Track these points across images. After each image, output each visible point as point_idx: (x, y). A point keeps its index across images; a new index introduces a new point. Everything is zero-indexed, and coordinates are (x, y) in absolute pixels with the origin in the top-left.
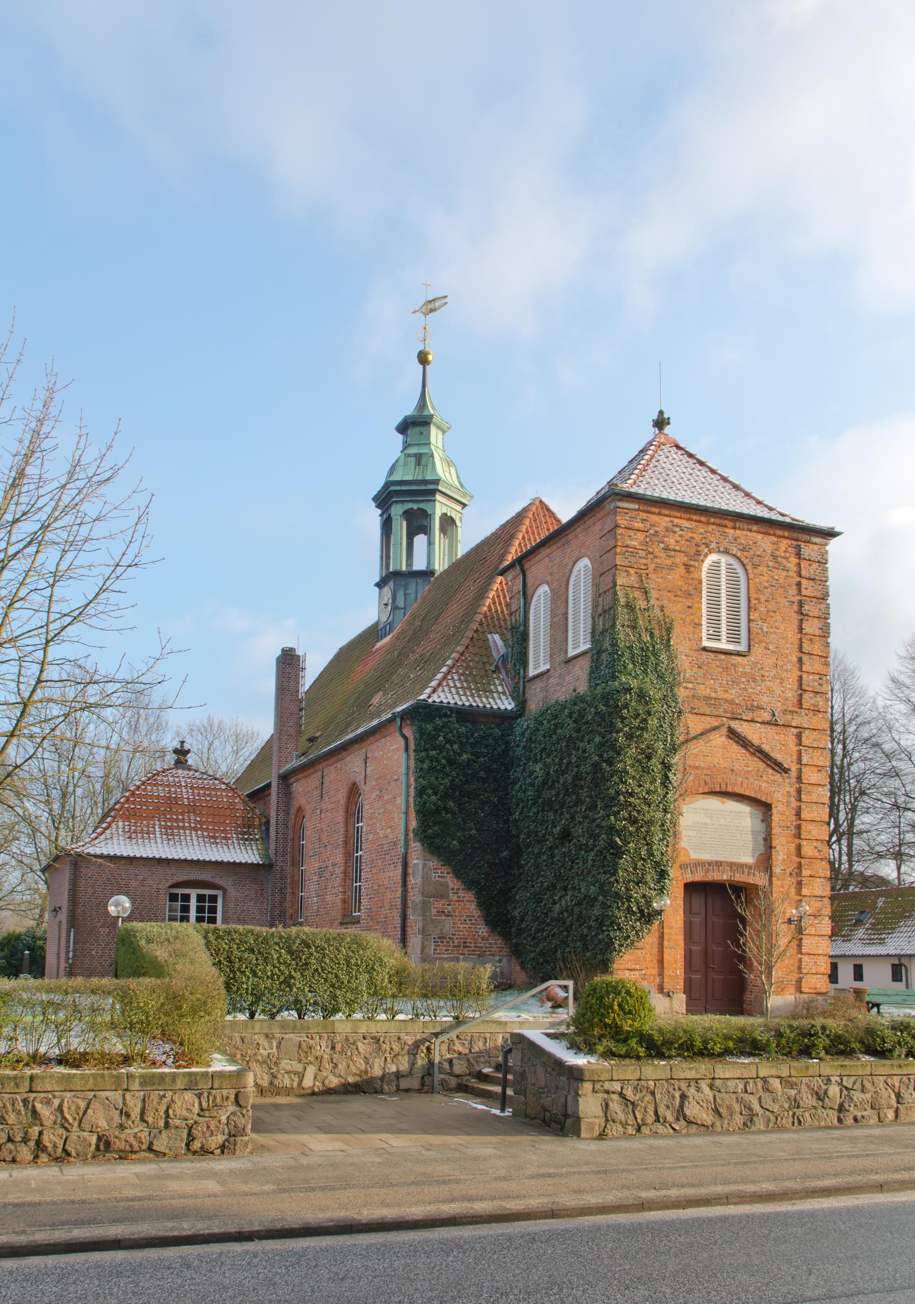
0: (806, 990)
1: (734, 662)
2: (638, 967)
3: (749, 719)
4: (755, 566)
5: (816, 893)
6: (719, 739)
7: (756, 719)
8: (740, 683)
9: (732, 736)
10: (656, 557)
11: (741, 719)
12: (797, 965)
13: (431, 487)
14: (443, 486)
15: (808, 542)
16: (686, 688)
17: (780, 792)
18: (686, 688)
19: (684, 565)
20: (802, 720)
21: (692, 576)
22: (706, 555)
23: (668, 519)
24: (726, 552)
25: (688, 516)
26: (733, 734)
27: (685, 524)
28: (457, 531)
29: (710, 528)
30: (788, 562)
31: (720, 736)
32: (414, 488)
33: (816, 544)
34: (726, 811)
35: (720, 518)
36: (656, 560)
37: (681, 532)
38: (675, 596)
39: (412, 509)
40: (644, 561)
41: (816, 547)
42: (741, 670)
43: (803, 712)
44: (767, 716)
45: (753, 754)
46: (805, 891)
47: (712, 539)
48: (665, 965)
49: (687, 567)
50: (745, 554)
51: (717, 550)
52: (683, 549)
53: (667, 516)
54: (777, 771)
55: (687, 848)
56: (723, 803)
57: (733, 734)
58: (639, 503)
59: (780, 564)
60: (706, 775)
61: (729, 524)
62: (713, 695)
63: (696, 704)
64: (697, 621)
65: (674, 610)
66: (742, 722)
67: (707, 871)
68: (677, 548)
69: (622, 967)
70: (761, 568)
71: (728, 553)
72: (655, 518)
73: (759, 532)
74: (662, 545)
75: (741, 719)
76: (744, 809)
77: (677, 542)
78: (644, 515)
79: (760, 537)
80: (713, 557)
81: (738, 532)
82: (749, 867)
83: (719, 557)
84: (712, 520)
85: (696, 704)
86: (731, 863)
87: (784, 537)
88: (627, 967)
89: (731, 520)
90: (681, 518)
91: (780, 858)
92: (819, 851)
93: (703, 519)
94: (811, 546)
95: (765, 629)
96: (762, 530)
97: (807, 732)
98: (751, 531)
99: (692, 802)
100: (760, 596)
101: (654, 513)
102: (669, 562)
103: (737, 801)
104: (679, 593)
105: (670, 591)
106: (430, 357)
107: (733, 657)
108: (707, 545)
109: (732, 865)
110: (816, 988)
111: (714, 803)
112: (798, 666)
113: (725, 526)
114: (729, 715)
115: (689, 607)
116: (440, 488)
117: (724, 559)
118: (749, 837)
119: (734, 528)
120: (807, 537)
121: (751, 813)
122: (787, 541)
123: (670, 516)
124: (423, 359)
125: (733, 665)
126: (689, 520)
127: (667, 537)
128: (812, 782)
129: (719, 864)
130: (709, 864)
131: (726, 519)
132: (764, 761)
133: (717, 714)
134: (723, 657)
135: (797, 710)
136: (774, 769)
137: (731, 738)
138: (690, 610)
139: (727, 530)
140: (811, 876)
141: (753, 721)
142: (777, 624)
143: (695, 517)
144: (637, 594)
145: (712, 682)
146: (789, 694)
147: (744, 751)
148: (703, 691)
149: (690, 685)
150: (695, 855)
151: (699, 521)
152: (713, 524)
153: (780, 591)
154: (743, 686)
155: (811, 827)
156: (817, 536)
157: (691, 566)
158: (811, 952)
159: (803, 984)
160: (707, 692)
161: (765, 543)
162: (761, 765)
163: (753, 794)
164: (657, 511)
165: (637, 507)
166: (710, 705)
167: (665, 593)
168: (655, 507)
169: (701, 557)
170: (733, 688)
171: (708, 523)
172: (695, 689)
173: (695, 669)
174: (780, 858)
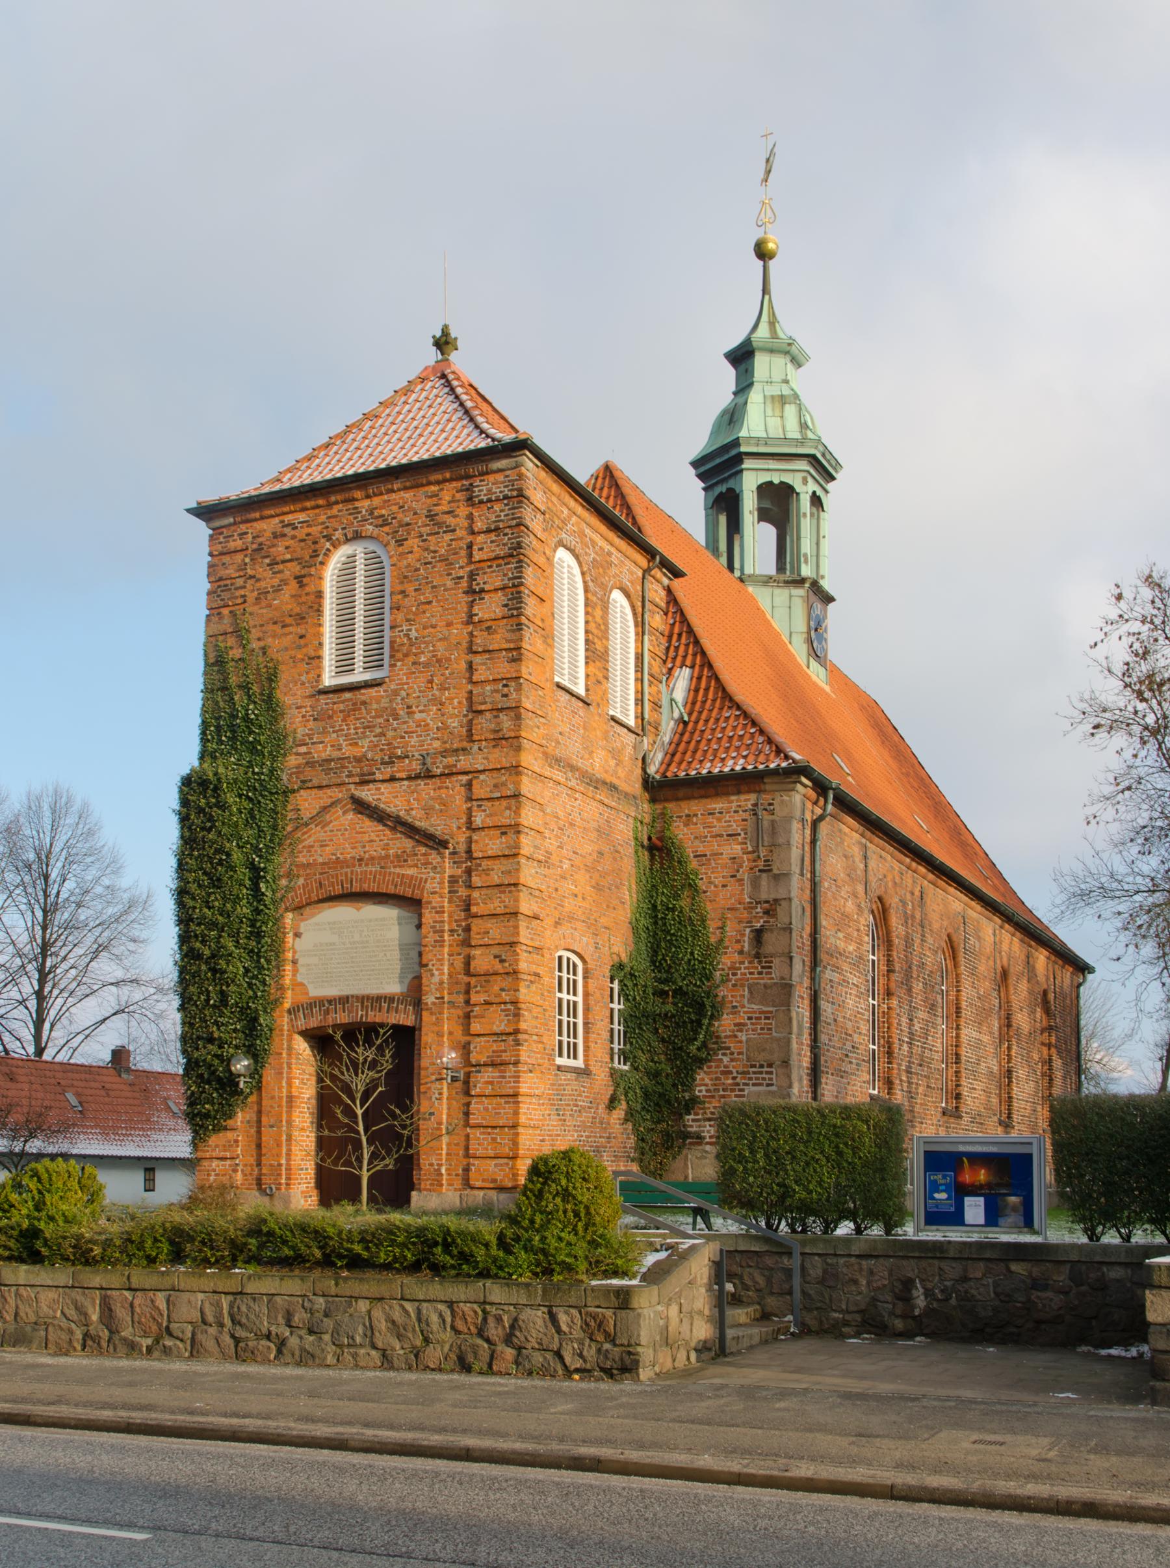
0: (478, 1184)
1: (363, 698)
2: (228, 1155)
3: (387, 777)
4: (400, 543)
5: (496, 1029)
6: (347, 818)
7: (398, 775)
8: (374, 726)
9: (361, 809)
10: (259, 580)
11: (375, 781)
12: (463, 1143)
13: (733, 452)
14: (748, 444)
15: (487, 473)
16: (297, 754)
17: (435, 877)
18: (297, 754)
19: (296, 578)
20: (476, 760)
21: (307, 589)
22: (328, 553)
23: (277, 520)
24: (357, 537)
25: (299, 506)
26: (361, 807)
27: (302, 517)
28: (798, 500)
29: (334, 511)
30: (455, 517)
31: (344, 813)
32: (718, 461)
33: (500, 471)
34: (362, 921)
35: (343, 490)
36: (258, 585)
37: (293, 533)
38: (283, 627)
39: (771, 483)
40: (242, 592)
41: (500, 477)
42: (375, 706)
43: (475, 747)
44: (416, 766)
45: (393, 829)
46: (476, 1027)
47: (336, 525)
48: (264, 1151)
49: (299, 578)
50: (386, 529)
51: (343, 539)
52: (296, 556)
53: (273, 516)
54: (432, 848)
55: (305, 982)
56: (358, 909)
57: (361, 807)
58: (234, 515)
59: (439, 524)
60: (321, 874)
61: (358, 494)
62: (336, 754)
63: (309, 773)
64: (313, 654)
65: (278, 644)
66: (379, 785)
67: (327, 1012)
68: (288, 556)
69: (208, 1155)
70: (410, 542)
71: (362, 537)
72: (259, 526)
73: (405, 488)
74: (267, 561)
75: (375, 781)
76: (389, 914)
77: (287, 548)
78: (243, 527)
79: (407, 495)
80: (344, 551)
81: (376, 501)
82: (390, 999)
83: (354, 547)
84: (333, 499)
85: (309, 773)
86: (363, 997)
87: (445, 481)
88: (214, 1155)
89: (359, 488)
90: (291, 512)
91: (436, 979)
92: (502, 961)
93: (321, 502)
94: (491, 478)
95: (413, 634)
96: (408, 484)
97: (482, 777)
98: (393, 491)
99: (313, 915)
100: (406, 585)
101: (256, 520)
102: (276, 582)
103: (380, 903)
104: (289, 620)
105: (275, 623)
106: (771, 246)
107: (363, 691)
108: (328, 538)
109: (362, 999)
110: (494, 1181)
111: (343, 912)
112: (467, 675)
113: (354, 500)
114: (357, 780)
115: (301, 637)
116: (743, 449)
117: (358, 550)
118: (396, 955)
119: (368, 497)
120: (481, 467)
121: (399, 918)
122: (455, 484)
123: (278, 515)
124: (762, 253)
125: (364, 703)
126: (304, 509)
127: (273, 546)
128: (490, 853)
129: (344, 1000)
130: (330, 1002)
131: (351, 489)
132: (411, 837)
133: (339, 781)
134: (348, 695)
135: (465, 744)
136: (427, 845)
137: (361, 813)
138: (302, 641)
139: (357, 504)
140: (487, 1003)
141: (392, 779)
142: (434, 621)
143: (308, 504)
144: (231, 641)
145: (335, 735)
146: (454, 723)
147: (381, 828)
148: (322, 752)
149: (303, 749)
150: (316, 992)
151: (318, 507)
152: (337, 503)
153: (440, 567)
154: (378, 730)
155: (490, 924)
156: (499, 459)
157: (304, 576)
158: (484, 1123)
159: (472, 1175)
160: (329, 752)
161: (410, 501)
162: (408, 844)
163: (391, 890)
164: (257, 515)
165: (232, 520)
166: (327, 771)
167: (271, 627)
168: (254, 510)
169: (320, 558)
170: (365, 737)
171: (330, 505)
172: (310, 753)
173: (311, 724)
174: (436, 979)
